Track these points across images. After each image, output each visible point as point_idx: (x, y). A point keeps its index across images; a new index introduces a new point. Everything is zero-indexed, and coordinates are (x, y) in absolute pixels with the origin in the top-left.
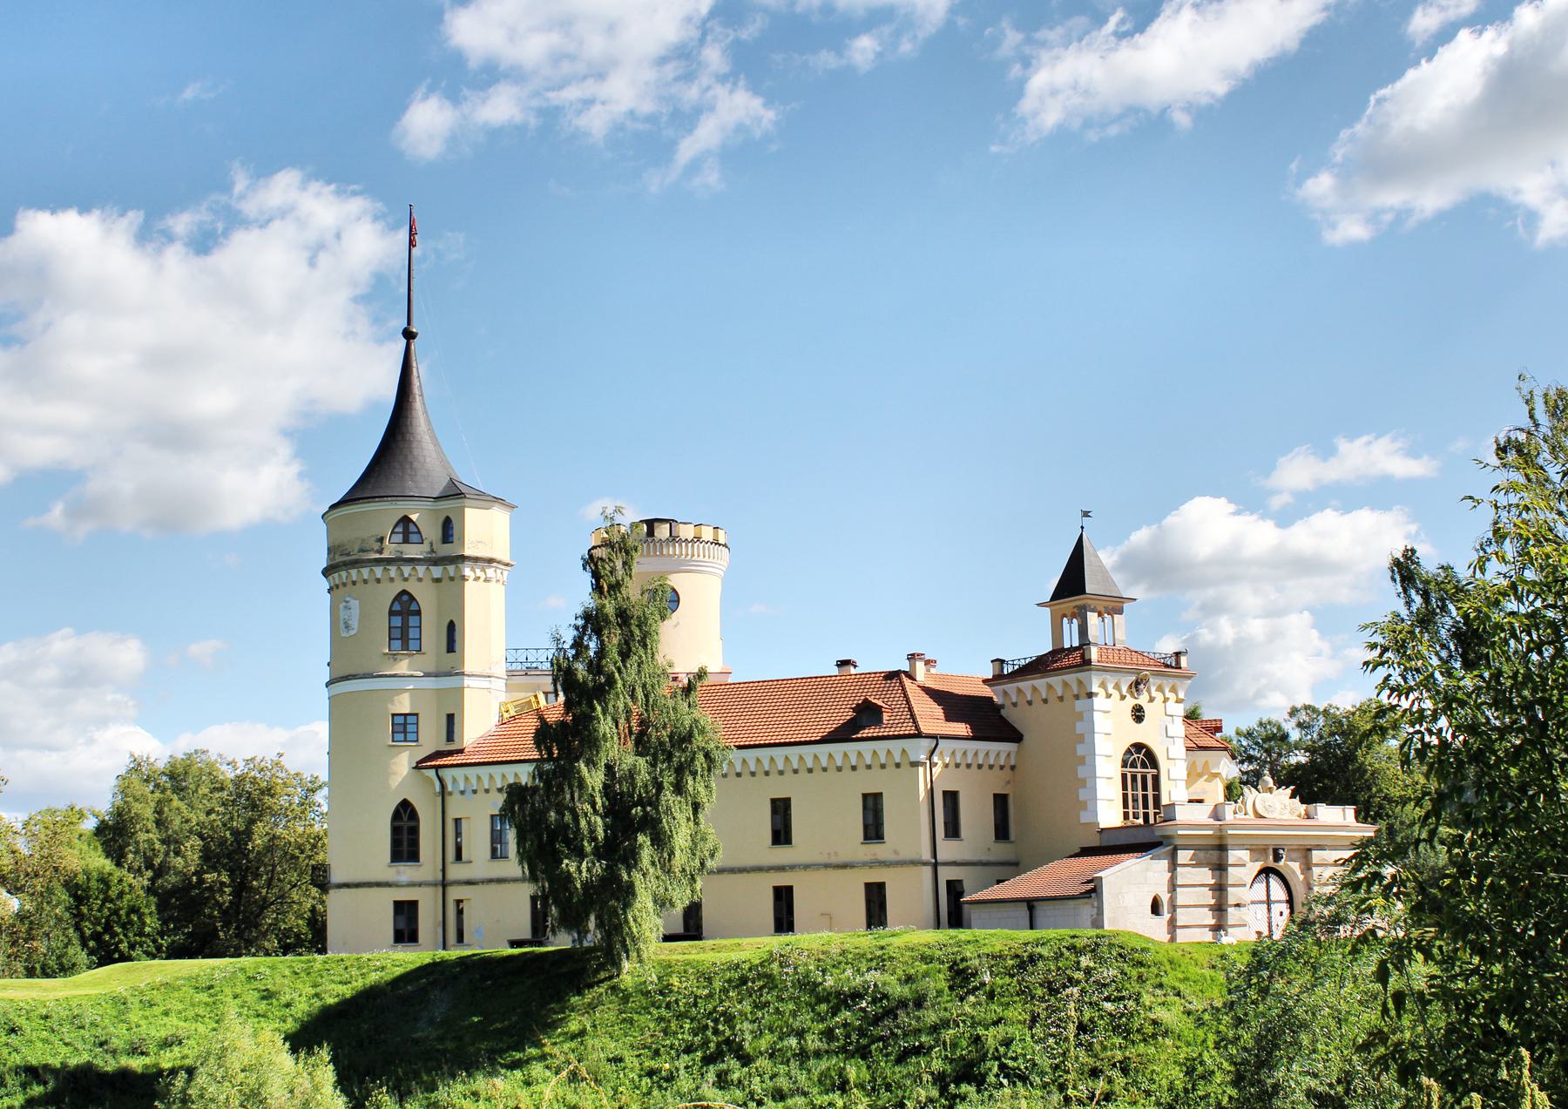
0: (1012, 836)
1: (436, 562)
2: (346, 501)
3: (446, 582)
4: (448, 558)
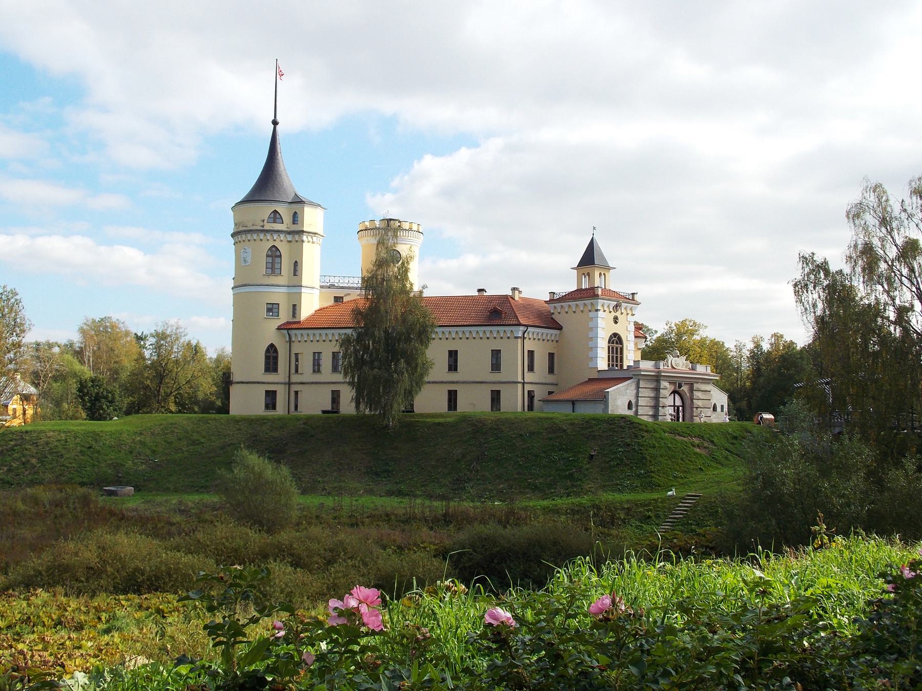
0: (555, 372)
1: (290, 233)
2: (243, 202)
3: (294, 242)
4: (297, 233)
